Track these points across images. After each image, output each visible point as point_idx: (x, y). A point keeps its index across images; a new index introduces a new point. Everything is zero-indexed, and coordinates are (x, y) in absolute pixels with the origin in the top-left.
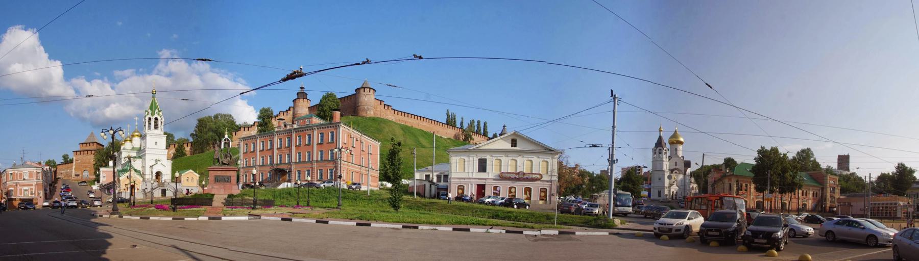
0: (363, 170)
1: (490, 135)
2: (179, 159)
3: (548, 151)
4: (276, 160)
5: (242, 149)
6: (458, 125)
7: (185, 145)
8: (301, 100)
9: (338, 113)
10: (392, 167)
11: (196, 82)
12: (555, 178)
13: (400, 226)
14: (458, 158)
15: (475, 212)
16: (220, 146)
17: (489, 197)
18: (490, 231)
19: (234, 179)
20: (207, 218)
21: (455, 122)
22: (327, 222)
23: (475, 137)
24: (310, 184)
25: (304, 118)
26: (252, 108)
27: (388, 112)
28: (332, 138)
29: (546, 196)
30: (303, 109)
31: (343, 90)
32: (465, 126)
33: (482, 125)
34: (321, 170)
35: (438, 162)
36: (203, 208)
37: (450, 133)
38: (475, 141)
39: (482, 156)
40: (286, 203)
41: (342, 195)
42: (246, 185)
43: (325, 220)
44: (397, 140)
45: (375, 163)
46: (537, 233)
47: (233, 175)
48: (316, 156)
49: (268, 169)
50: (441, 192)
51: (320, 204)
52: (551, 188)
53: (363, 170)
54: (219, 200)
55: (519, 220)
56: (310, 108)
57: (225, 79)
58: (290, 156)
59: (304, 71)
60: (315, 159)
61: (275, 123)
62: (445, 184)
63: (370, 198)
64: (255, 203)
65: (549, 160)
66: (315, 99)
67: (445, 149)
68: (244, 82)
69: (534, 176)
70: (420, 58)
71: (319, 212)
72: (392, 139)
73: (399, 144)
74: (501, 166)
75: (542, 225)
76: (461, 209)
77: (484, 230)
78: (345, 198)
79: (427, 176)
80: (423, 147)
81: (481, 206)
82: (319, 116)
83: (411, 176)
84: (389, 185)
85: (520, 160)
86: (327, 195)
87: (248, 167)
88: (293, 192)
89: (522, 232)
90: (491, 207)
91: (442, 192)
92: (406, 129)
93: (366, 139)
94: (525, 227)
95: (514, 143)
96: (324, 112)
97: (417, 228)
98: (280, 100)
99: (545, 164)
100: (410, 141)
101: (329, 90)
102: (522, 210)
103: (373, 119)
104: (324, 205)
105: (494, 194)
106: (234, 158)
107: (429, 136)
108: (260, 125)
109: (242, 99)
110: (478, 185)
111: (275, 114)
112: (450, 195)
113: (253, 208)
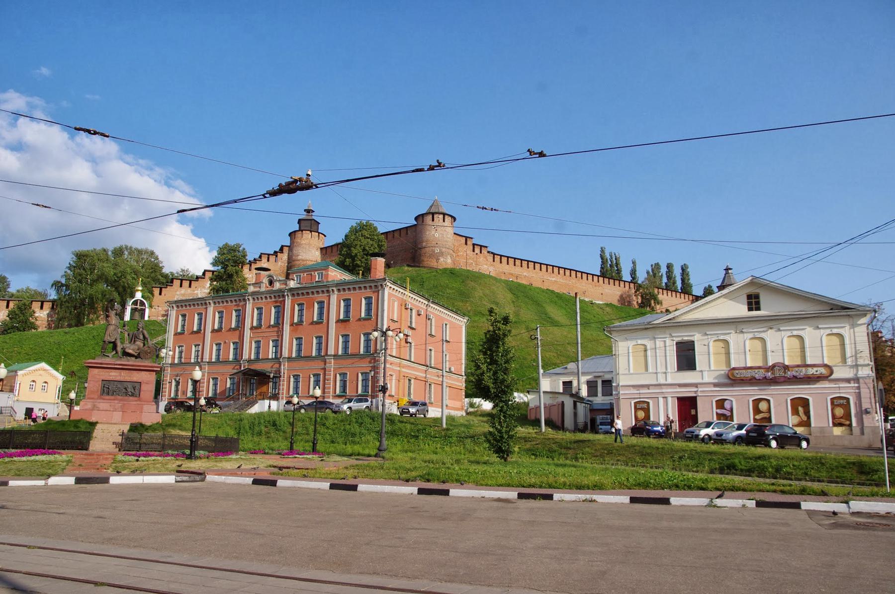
0: (432, 375)
1: (698, 291)
2: (16, 335)
3: (840, 310)
4: (248, 352)
5: (174, 324)
6: (626, 276)
7: (36, 306)
8: (307, 234)
9: (381, 261)
10: (492, 368)
11: (80, 173)
12: (867, 372)
13: (512, 494)
14: (631, 344)
15: (678, 459)
16: (121, 315)
17: (708, 425)
18: (719, 502)
19: (149, 389)
20: (70, 481)
21: (619, 271)
22: (354, 488)
23: (663, 297)
24: (320, 405)
25: (310, 270)
26: (201, 242)
27: (481, 259)
28: (369, 310)
29: (848, 416)
30: (310, 251)
31: (390, 214)
32: (641, 277)
33: (677, 272)
34: (344, 375)
35: (587, 354)
36: (62, 457)
37: (610, 293)
38: (665, 305)
39: (685, 336)
40: (264, 444)
41: (387, 427)
42: (177, 404)
43: (350, 481)
44: (501, 312)
45: (457, 359)
46: (840, 507)
47: (147, 380)
48: (334, 345)
49: (230, 370)
50: (599, 418)
51: (340, 447)
52: (859, 396)
53: (432, 375)
54: (107, 435)
55: (788, 476)
56: (324, 251)
57: (146, 178)
58: (278, 344)
59: (314, 180)
60: (331, 351)
61: (249, 275)
62: (607, 400)
63: (447, 433)
64: (194, 445)
65: (846, 331)
66: (335, 234)
67: (601, 328)
68: (187, 188)
69: (811, 371)
70: (541, 155)
71: (336, 464)
72: (491, 311)
73: (506, 320)
74: (728, 354)
75: (848, 488)
76: (645, 454)
77: (704, 501)
78: (393, 434)
79: (567, 385)
80: (555, 323)
81: (692, 445)
82: (342, 265)
83: (533, 386)
84: (487, 406)
85: (772, 337)
86: (356, 428)
87: (184, 365)
88: (282, 422)
89: (797, 506)
90: (714, 447)
91: (600, 418)
92: (519, 291)
93: (436, 311)
94: (803, 491)
95: (753, 302)
96: (353, 258)
97: (549, 497)
98: (262, 232)
99: (836, 341)
100: (527, 314)
101: (364, 218)
102: (790, 451)
103: (452, 273)
104: (349, 449)
105: (719, 416)
106: (152, 342)
107: (567, 301)
108: (216, 277)
109: (182, 222)
110: (681, 400)
111: (250, 258)
112: (619, 424)
113: (189, 457)
